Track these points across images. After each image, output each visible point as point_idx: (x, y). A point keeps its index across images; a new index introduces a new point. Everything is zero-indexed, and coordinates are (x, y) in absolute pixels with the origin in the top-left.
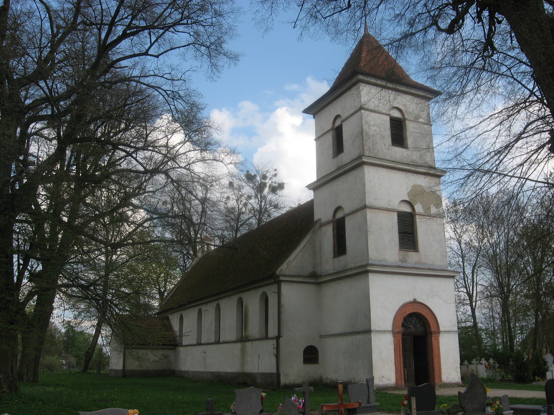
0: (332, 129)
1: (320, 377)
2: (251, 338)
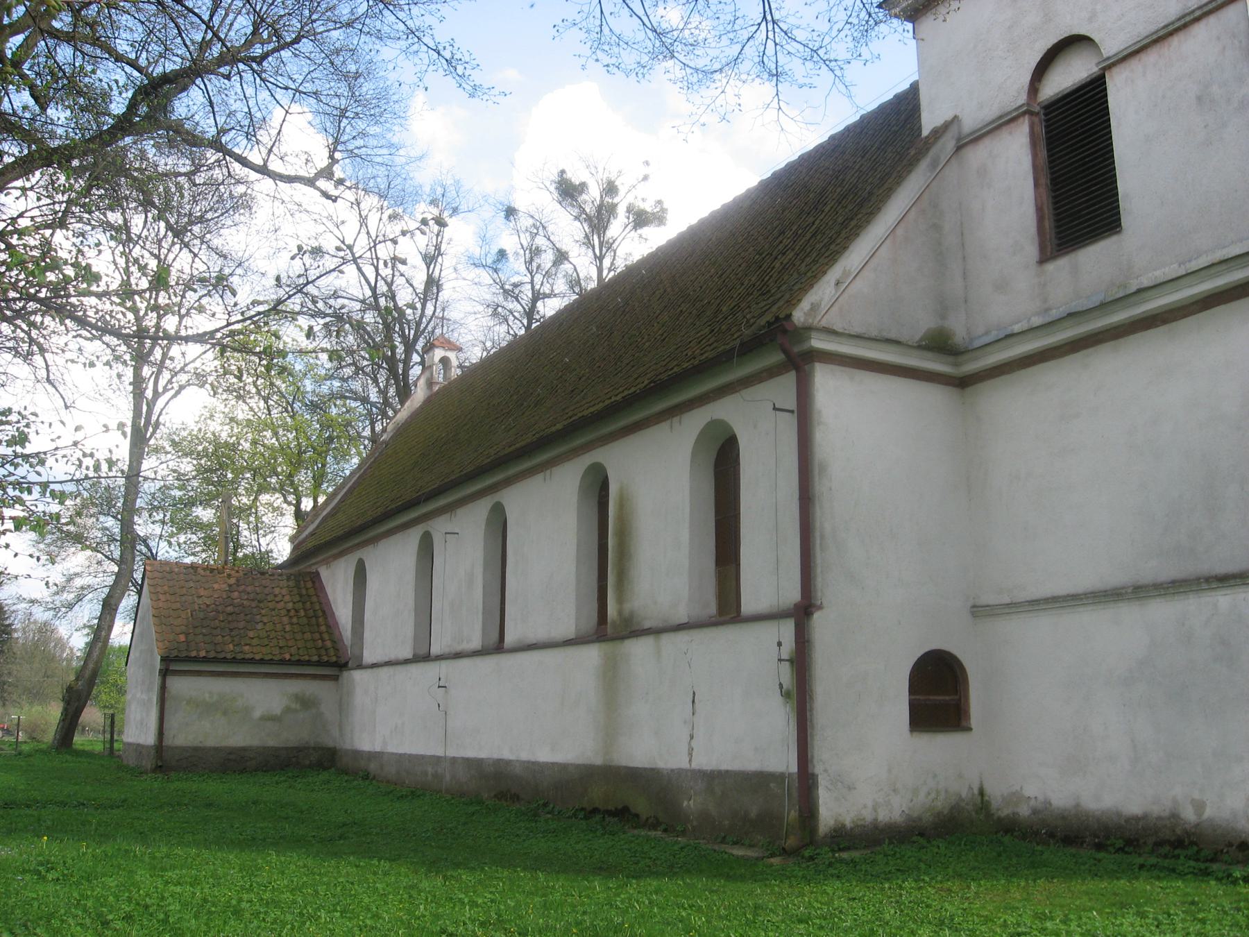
1: (976, 791)
2: (647, 625)
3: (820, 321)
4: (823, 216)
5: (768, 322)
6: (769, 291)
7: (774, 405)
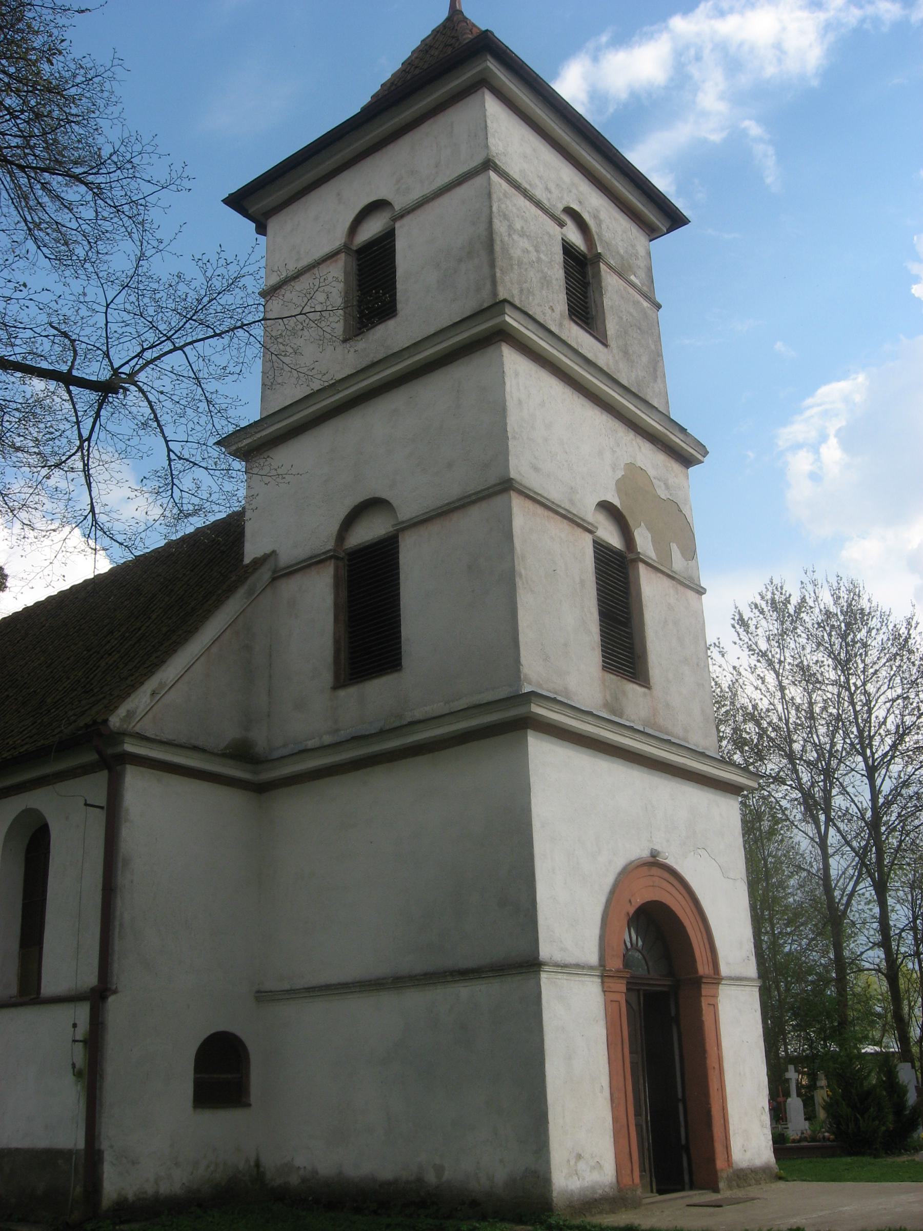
0: (346, 248)
1: (252, 1163)
3: (134, 726)
4: (148, 623)
5: (86, 724)
6: (92, 690)
7: (86, 800)
